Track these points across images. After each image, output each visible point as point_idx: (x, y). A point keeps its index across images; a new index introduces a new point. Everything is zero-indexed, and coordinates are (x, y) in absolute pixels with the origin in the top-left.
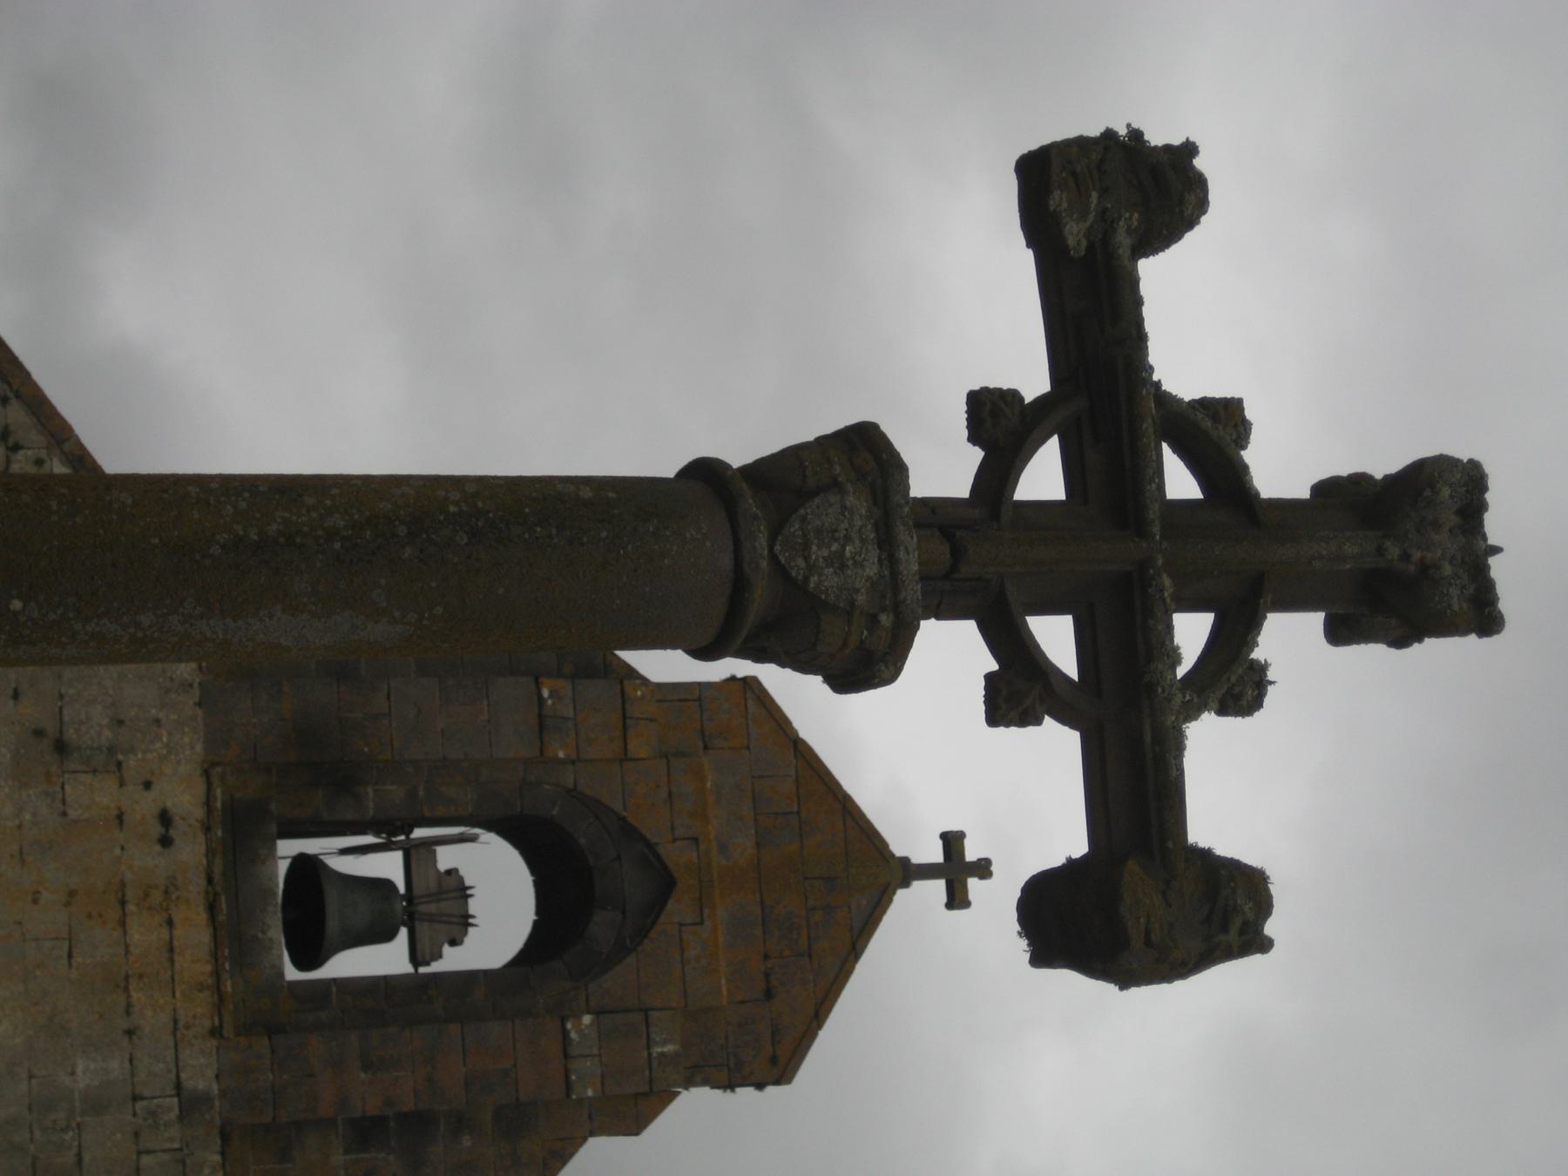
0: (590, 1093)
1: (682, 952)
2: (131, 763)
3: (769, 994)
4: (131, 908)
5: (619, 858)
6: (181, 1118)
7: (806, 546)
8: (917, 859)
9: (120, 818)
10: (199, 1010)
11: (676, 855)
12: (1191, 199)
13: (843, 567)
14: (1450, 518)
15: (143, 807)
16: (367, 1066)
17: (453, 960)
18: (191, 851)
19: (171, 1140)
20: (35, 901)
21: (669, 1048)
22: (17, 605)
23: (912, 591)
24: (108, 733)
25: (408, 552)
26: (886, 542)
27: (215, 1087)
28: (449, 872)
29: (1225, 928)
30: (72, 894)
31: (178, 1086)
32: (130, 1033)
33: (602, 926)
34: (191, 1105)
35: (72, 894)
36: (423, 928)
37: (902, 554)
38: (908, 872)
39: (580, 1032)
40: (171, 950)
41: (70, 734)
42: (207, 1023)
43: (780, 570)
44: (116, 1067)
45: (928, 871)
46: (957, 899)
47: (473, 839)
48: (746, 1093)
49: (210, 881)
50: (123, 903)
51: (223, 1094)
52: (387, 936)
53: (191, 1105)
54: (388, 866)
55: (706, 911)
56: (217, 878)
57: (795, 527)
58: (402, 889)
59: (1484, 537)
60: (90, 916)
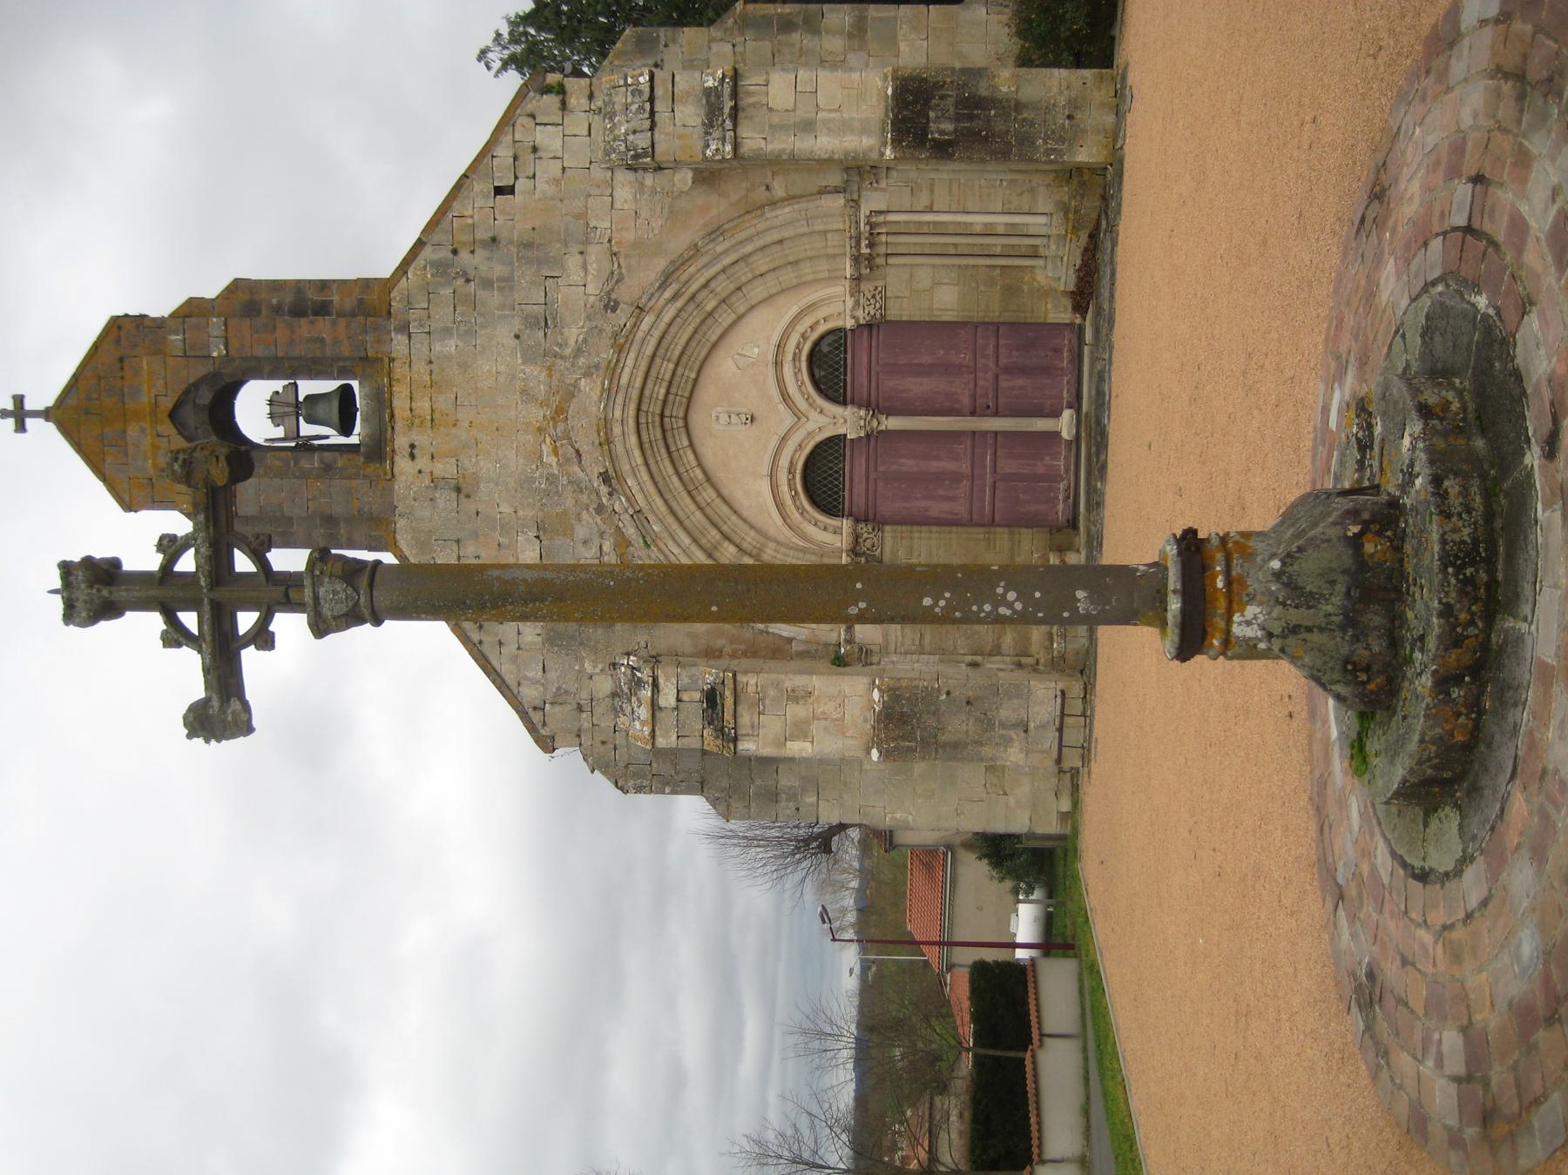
0: (215, 320)
1: (166, 383)
2: (427, 482)
3: (121, 360)
4: (429, 418)
5: (196, 428)
6: (409, 323)
7: (347, 598)
8: (41, 421)
9: (433, 458)
10: (399, 370)
11: (167, 428)
12: (191, 719)
13: (333, 591)
14: (79, 605)
15: (422, 462)
16: (322, 340)
17: (278, 385)
18: (401, 442)
19: (413, 313)
20: (471, 422)
21: (173, 337)
22: (612, 583)
23: (307, 582)
24: (438, 495)
25: (487, 597)
26: (316, 599)
27: (393, 335)
28: (278, 425)
29: (184, 460)
30: (455, 425)
31: (410, 337)
32: (431, 362)
33: (205, 397)
34: (404, 328)
35: (455, 425)
36: (292, 400)
37: (311, 595)
38: (46, 414)
39: (219, 349)
40: (411, 398)
41: (454, 495)
42: (396, 364)
43: (356, 590)
44: (437, 347)
45: (35, 414)
46: (19, 400)
47: (267, 440)
48: (133, 312)
49: (393, 428)
50: (432, 420)
51: (389, 332)
52: (308, 398)
53: (404, 328)
54: (307, 429)
55: (153, 401)
56: (390, 428)
57: (351, 604)
58: (301, 418)
59: (63, 597)
60: (447, 415)
